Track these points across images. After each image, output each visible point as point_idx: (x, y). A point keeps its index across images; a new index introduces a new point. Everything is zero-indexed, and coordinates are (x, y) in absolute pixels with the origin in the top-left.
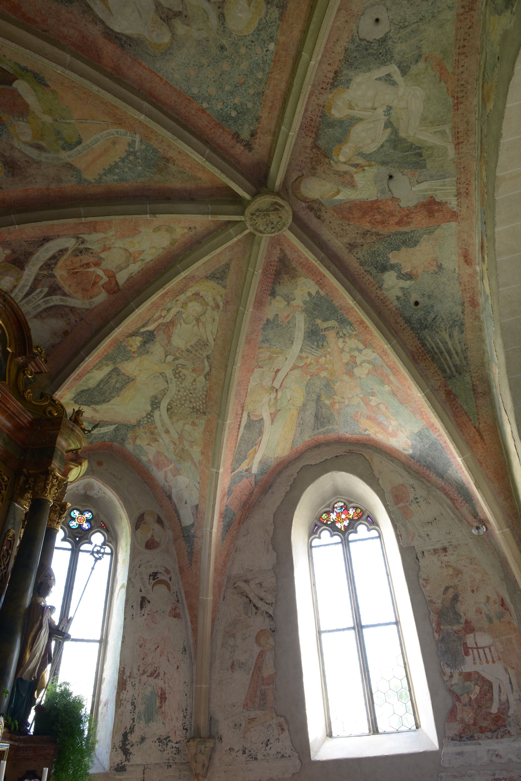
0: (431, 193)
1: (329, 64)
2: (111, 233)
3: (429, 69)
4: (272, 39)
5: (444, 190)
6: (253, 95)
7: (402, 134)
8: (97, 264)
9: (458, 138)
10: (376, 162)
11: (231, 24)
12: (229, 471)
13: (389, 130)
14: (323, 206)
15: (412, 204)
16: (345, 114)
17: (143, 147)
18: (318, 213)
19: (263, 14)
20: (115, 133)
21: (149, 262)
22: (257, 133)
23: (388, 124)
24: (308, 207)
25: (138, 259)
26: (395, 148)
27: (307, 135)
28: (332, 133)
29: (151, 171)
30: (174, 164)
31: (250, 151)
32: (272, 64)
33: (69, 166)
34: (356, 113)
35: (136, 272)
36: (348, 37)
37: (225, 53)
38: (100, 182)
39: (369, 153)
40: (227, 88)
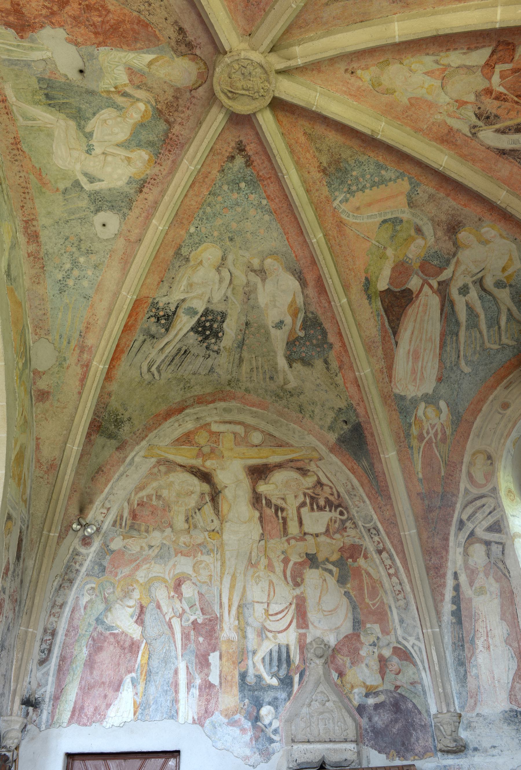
0: (24, 44)
1: (146, 199)
2: (439, 117)
3: (53, 182)
4: (191, 235)
5: (6, 44)
6: (219, 195)
7: (72, 123)
8: (489, 91)
9: (5, 108)
10: (101, 96)
11: (219, 254)
13: (88, 129)
14: (172, 48)
15: (47, 32)
16: (135, 153)
17: (337, 193)
18: (181, 37)
19: (193, 253)
20: (351, 216)
21: (433, 54)
22: (228, 157)
23: (89, 136)
24: (193, 48)
25: (441, 67)
26: (79, 110)
27: (177, 136)
28: (150, 136)
29: (347, 166)
30: (321, 163)
31: (241, 142)
32: (195, 216)
33: (411, 204)
34: (123, 153)
35: (457, 52)
36: (129, 219)
37: (230, 235)
38: (401, 173)
39: (109, 109)
40: (239, 209)
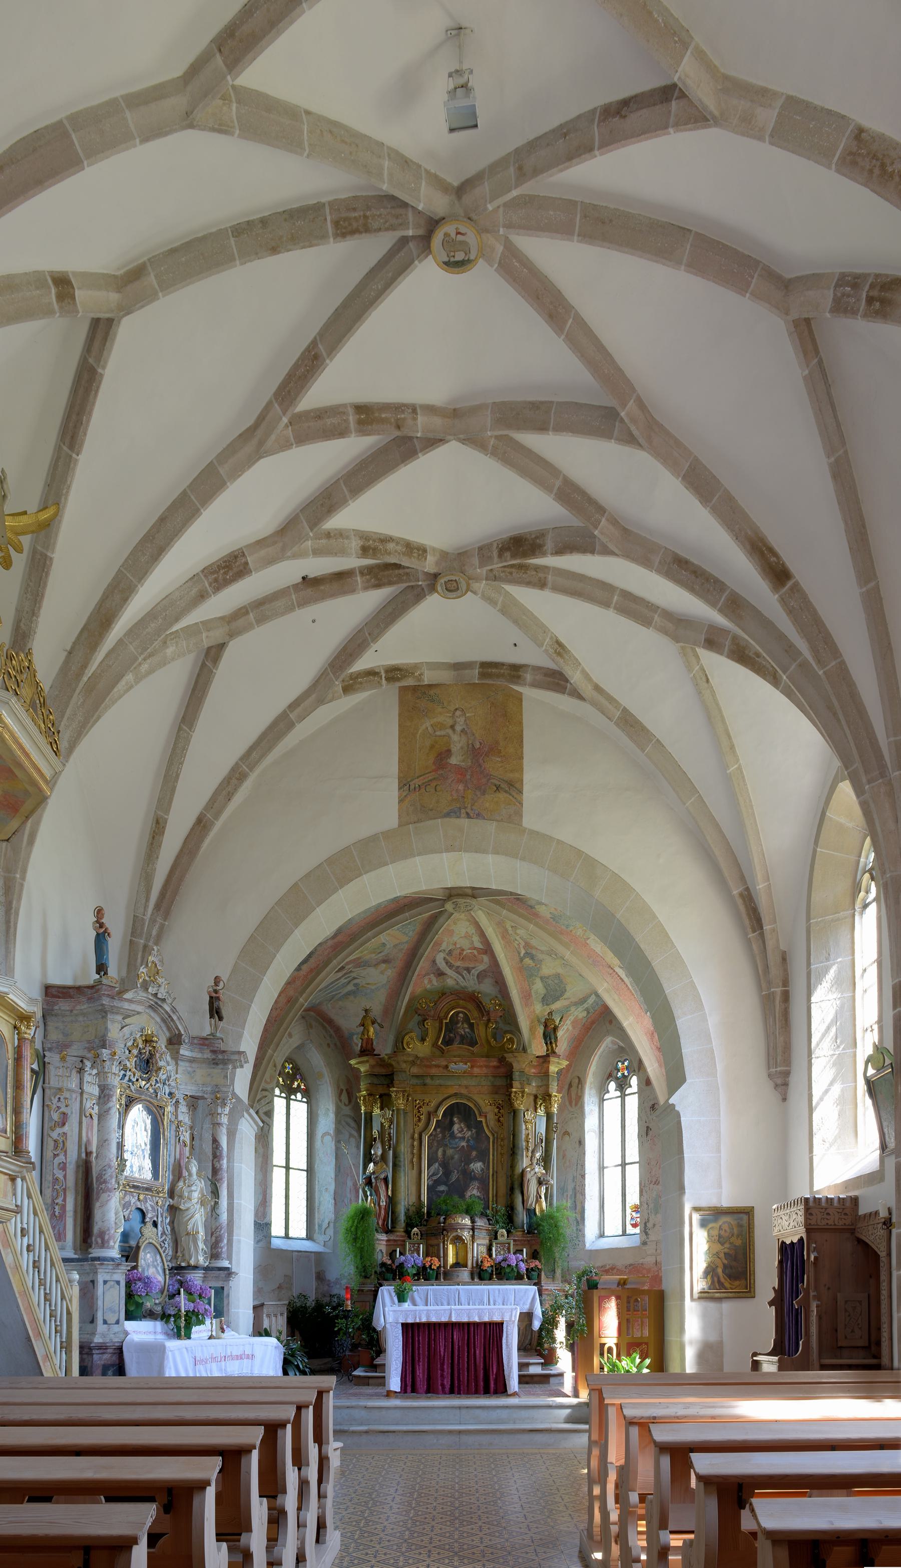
8: (463, 950)
12: (643, 1014)
